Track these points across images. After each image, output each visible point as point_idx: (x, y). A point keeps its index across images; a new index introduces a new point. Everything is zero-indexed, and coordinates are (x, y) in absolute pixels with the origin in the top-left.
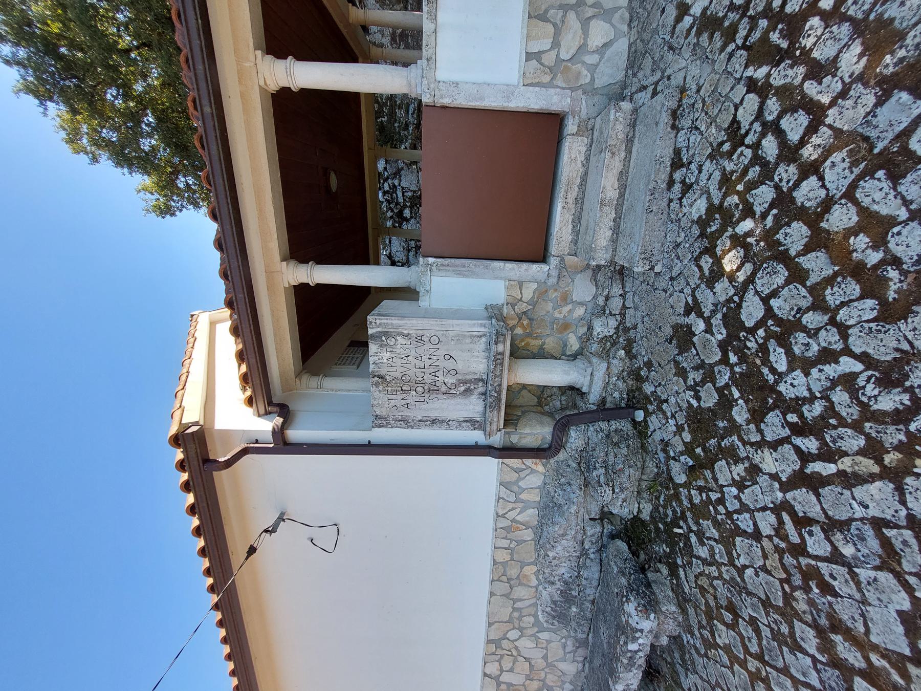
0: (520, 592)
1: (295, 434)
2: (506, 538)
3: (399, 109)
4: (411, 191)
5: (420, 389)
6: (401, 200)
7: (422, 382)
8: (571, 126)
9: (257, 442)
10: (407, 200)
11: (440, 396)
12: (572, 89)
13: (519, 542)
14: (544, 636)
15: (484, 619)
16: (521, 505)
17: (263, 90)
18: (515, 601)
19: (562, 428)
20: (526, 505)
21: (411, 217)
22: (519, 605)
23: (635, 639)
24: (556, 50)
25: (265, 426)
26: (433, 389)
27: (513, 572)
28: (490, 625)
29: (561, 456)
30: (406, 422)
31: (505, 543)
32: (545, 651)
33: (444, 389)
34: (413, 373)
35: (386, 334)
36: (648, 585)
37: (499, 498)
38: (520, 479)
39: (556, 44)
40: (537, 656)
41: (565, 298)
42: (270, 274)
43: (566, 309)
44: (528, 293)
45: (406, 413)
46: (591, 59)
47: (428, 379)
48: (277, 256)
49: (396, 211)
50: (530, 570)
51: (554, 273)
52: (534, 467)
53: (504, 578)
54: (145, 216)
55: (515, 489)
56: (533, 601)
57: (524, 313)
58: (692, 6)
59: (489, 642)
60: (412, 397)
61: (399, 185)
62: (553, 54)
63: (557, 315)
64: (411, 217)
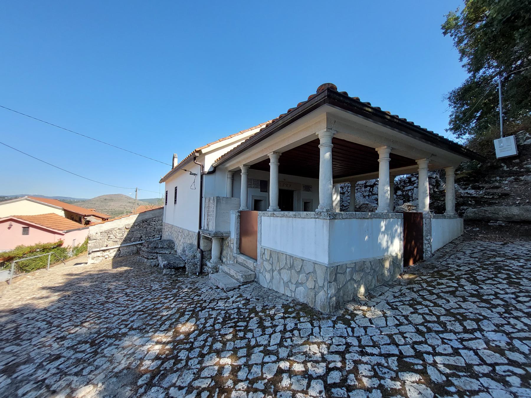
1: (204, 177)
3: (515, 179)
4: (412, 195)
6: (406, 188)
10: (407, 193)
21: (397, 196)
24: (425, 355)
25: (207, 169)
36: (170, 268)
42: (239, 162)
48: (244, 163)
49: (399, 186)
54: (444, 16)
61: (414, 187)
64: (397, 196)
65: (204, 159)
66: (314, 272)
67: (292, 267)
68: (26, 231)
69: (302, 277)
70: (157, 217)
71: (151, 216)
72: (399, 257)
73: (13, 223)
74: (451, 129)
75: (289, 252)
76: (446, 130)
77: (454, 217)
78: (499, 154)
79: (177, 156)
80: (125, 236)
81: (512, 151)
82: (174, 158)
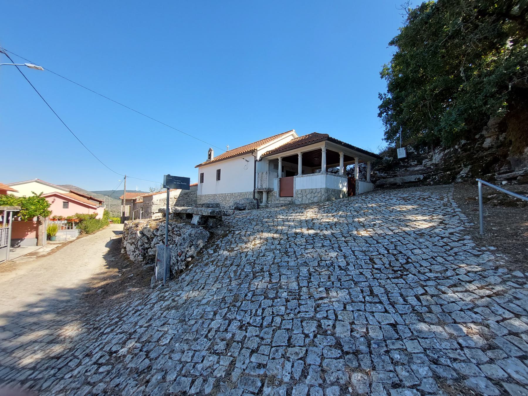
1: (257, 162)
9: (38, 330)
19: (257, 199)
20: (249, 196)
25: (258, 158)
27: (241, 196)
40: (230, 201)
42: (279, 155)
44: (275, 195)
48: (282, 156)
58: (519, 319)
65: (257, 153)
66: (321, 191)
67: (312, 192)
68: (66, 205)
69: (316, 194)
72: (346, 192)
73: (56, 198)
74: (385, 139)
76: (382, 139)
77: (369, 182)
78: (399, 157)
79: (212, 150)
80: (174, 203)
81: (404, 156)
82: (210, 150)
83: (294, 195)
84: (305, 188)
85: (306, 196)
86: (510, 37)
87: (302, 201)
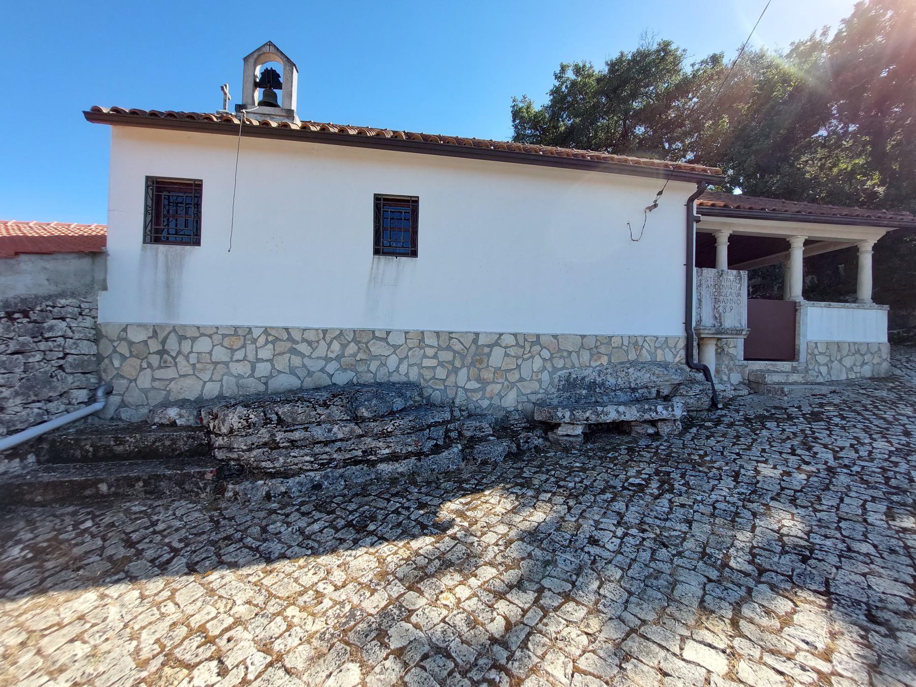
0: (585, 356)
2: (629, 343)
5: (716, 294)
7: (720, 295)
8: (795, 364)
11: (713, 304)
12: (807, 362)
13: (627, 352)
14: (545, 376)
15: (558, 332)
16: (653, 351)
17: (719, 231)
18: (578, 353)
22: (574, 355)
23: (666, 408)
26: (716, 300)
28: (555, 337)
29: (688, 369)
30: (700, 286)
31: (626, 343)
32: (529, 379)
33: (717, 306)
34: (724, 291)
35: (741, 278)
37: (657, 338)
38: (670, 349)
39: (820, 353)
41: (730, 370)
42: (730, 225)
43: (726, 370)
45: (704, 286)
46: (816, 368)
47: (721, 298)
50: (604, 360)
51: (741, 363)
52: (678, 356)
53: (598, 343)
55: (664, 346)
56: (577, 365)
57: (723, 350)
59: (538, 336)
60: (712, 290)
62: (817, 353)
63: (723, 366)
66: (879, 349)
67: (858, 351)
69: (867, 358)
70: (73, 295)
71: (46, 288)
75: (850, 339)
83: (803, 356)
84: (836, 339)
85: (840, 361)
86: (807, 176)
87: (829, 373)
